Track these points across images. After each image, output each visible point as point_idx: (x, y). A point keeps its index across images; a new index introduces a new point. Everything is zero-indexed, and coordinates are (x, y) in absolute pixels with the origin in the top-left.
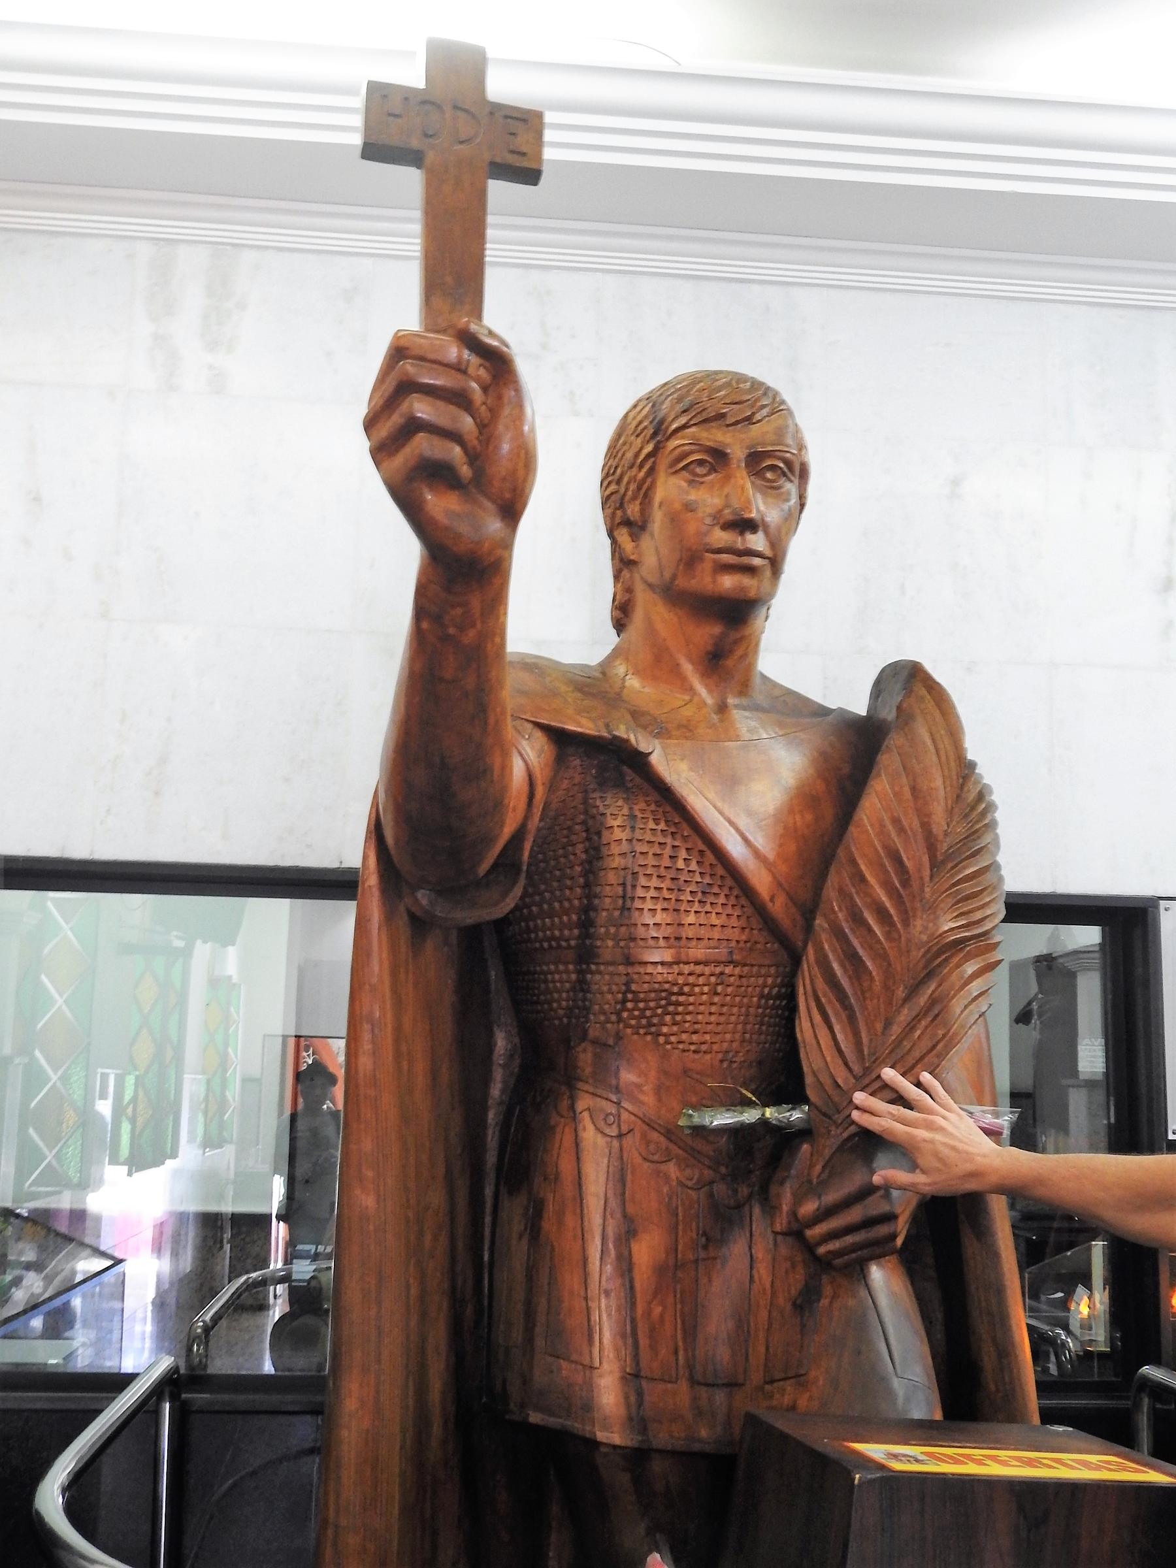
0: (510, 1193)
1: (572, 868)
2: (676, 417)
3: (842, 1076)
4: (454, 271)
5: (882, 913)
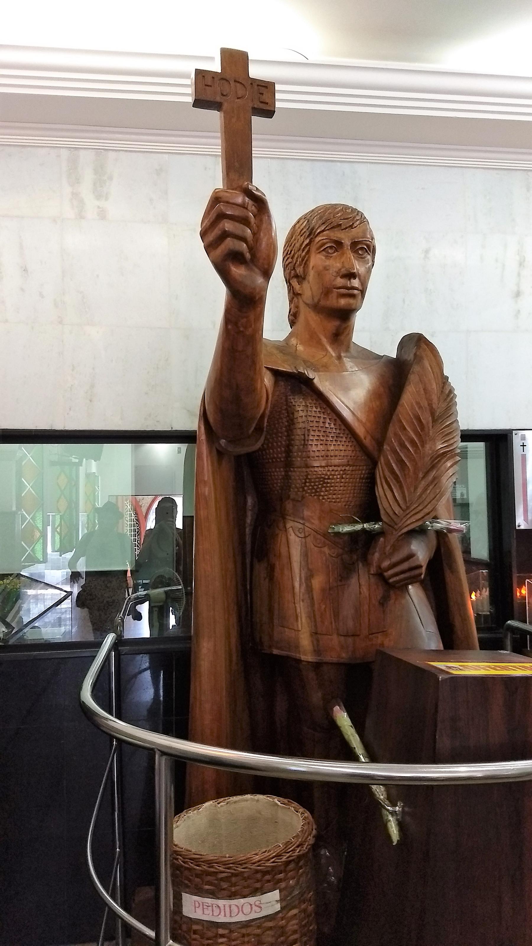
0: (259, 561)
1: (281, 428)
2: (319, 226)
3: (397, 510)
4: (238, 160)
5: (413, 442)
